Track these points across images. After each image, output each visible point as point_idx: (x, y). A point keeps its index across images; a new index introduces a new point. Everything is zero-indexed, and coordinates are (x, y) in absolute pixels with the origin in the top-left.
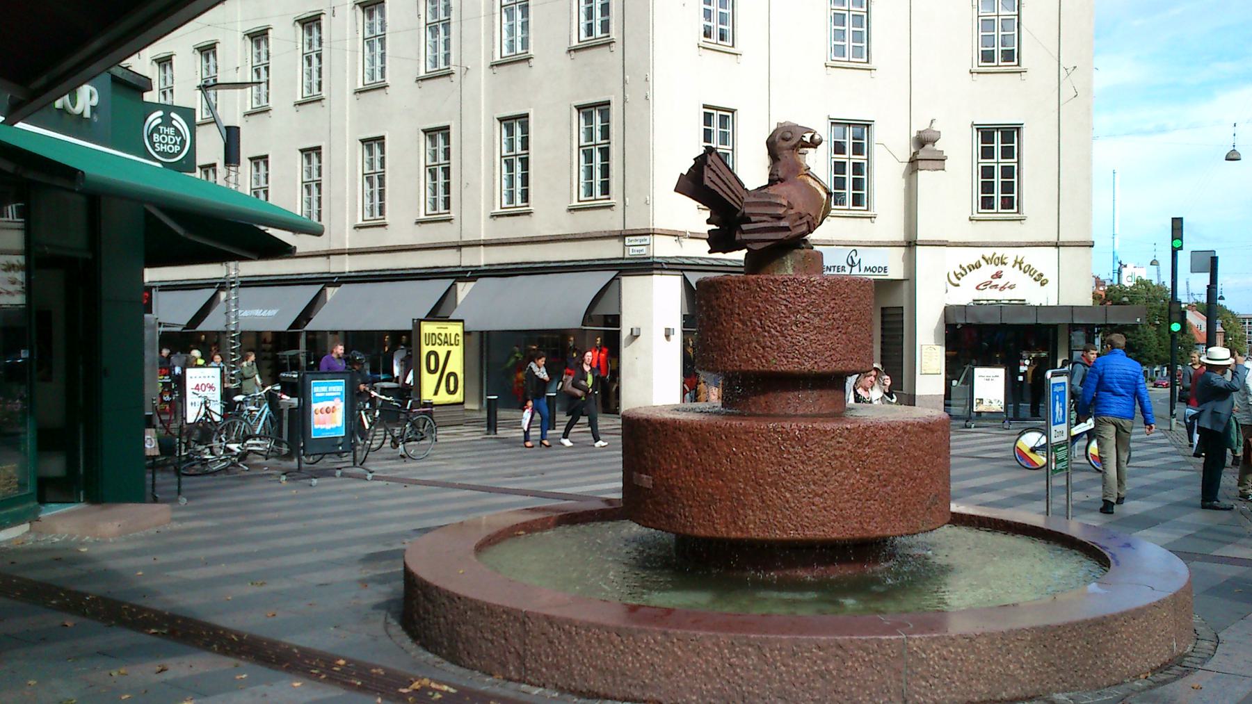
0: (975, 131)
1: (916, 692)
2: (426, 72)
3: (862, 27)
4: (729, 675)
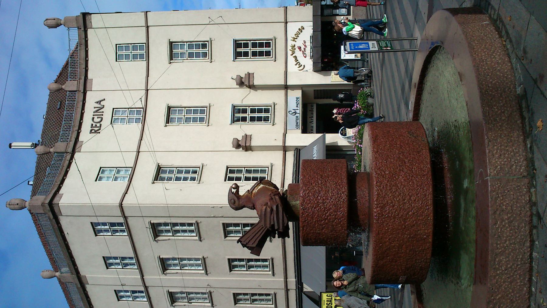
0: (237, 60)
1: (519, 171)
2: (209, 303)
3: (192, 110)
4: (512, 271)
